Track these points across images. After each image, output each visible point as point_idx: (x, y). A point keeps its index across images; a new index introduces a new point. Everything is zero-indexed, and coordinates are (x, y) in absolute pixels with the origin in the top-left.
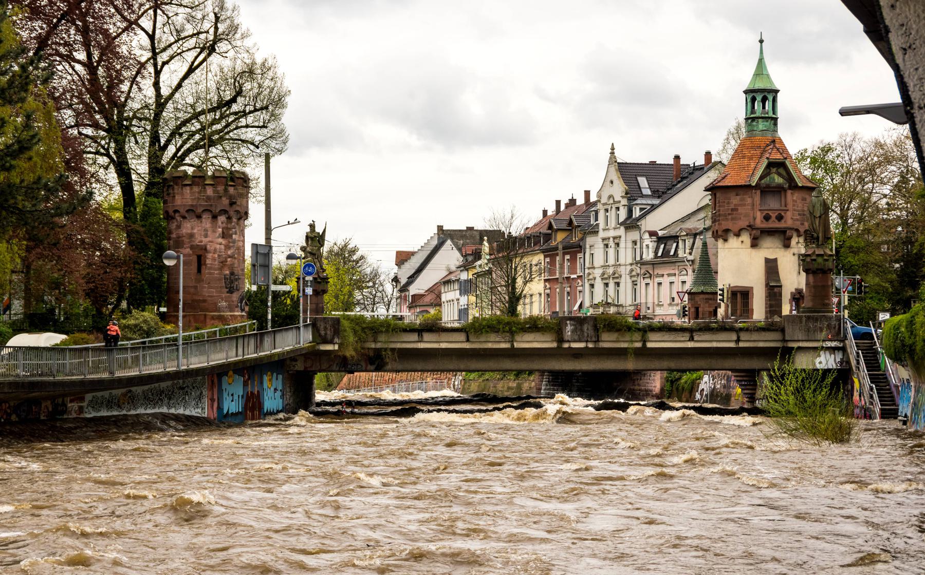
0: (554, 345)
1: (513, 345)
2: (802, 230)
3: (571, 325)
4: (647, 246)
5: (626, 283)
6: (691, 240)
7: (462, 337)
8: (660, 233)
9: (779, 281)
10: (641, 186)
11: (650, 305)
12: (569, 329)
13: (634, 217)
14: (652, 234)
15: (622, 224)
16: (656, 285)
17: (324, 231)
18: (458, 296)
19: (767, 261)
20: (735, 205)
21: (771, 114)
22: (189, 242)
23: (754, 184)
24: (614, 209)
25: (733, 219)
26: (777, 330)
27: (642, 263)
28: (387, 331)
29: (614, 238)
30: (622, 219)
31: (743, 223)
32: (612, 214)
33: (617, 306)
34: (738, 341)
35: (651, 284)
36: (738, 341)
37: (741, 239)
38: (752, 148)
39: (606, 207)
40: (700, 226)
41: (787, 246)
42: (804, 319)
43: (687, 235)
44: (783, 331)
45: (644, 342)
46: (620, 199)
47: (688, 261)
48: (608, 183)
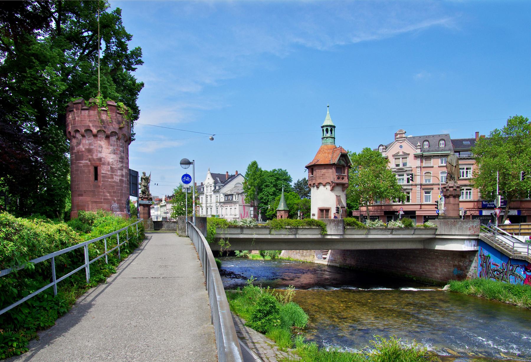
0: (319, 236)
17: (150, 175)
20: (324, 173)
25: (322, 179)
27: (220, 203)
29: (210, 195)
31: (329, 181)
32: (209, 188)
38: (328, 149)
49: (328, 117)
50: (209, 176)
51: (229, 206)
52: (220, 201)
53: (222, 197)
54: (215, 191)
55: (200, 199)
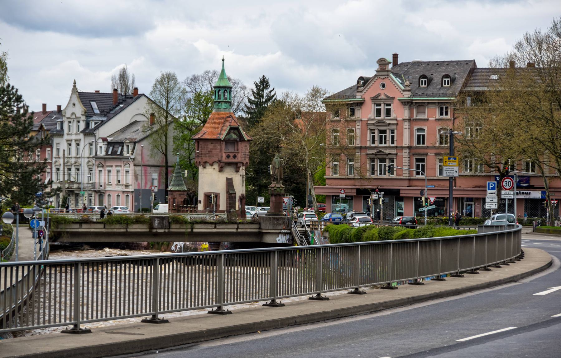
0: (148, 230)
1: (127, 230)
2: (245, 163)
3: (158, 221)
4: (101, 147)
6: (133, 146)
7: (102, 226)
8: (109, 139)
9: (234, 190)
10: (93, 107)
11: (103, 184)
12: (156, 222)
13: (90, 128)
14: (104, 140)
15: (82, 132)
16: (107, 172)
19: (228, 179)
20: (211, 149)
21: (228, 100)
23: (223, 139)
24: (75, 122)
25: (209, 156)
26: (257, 224)
27: (97, 157)
28: (65, 223)
29: (76, 140)
31: (217, 159)
32: (74, 125)
34: (237, 229)
35: (103, 172)
36: (237, 229)
37: (213, 167)
38: (219, 118)
39: (70, 120)
40: (139, 137)
41: (237, 171)
42: (272, 219)
44: (260, 224)
45: (192, 229)
46: (81, 116)
47: (131, 159)
48: (71, 105)
51: (114, 167)
54: (88, 132)
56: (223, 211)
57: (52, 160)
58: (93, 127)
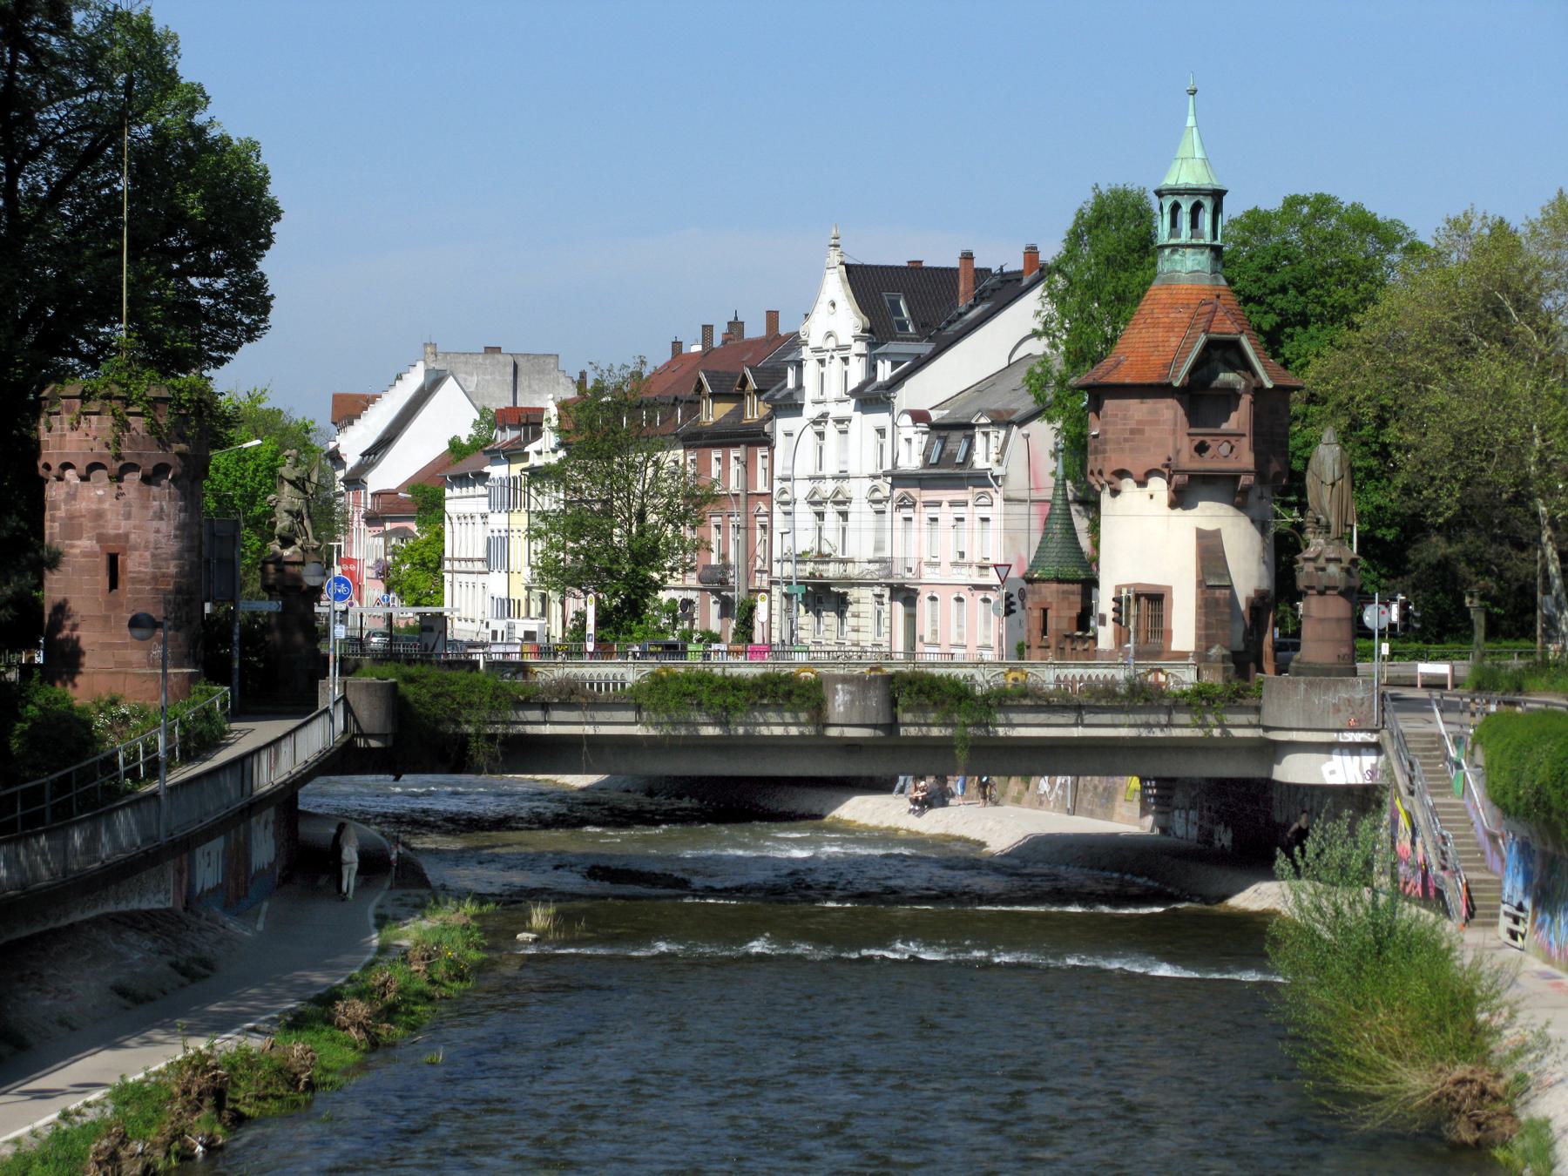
0: (809, 731)
5: (861, 511)
8: (935, 416)
14: (919, 416)
18: (485, 509)
19: (1201, 535)
20: (1139, 422)
22: (94, 528)
24: (837, 361)
30: (852, 385)
31: (1158, 462)
32: (834, 369)
33: (844, 562)
38: (1172, 306)
39: (820, 356)
43: (993, 424)
49: (1192, 145)
50: (835, 286)
51: (945, 505)
52: (895, 464)
53: (909, 441)
55: (780, 441)
56: (1183, 655)
57: (772, 487)
58: (887, 378)
